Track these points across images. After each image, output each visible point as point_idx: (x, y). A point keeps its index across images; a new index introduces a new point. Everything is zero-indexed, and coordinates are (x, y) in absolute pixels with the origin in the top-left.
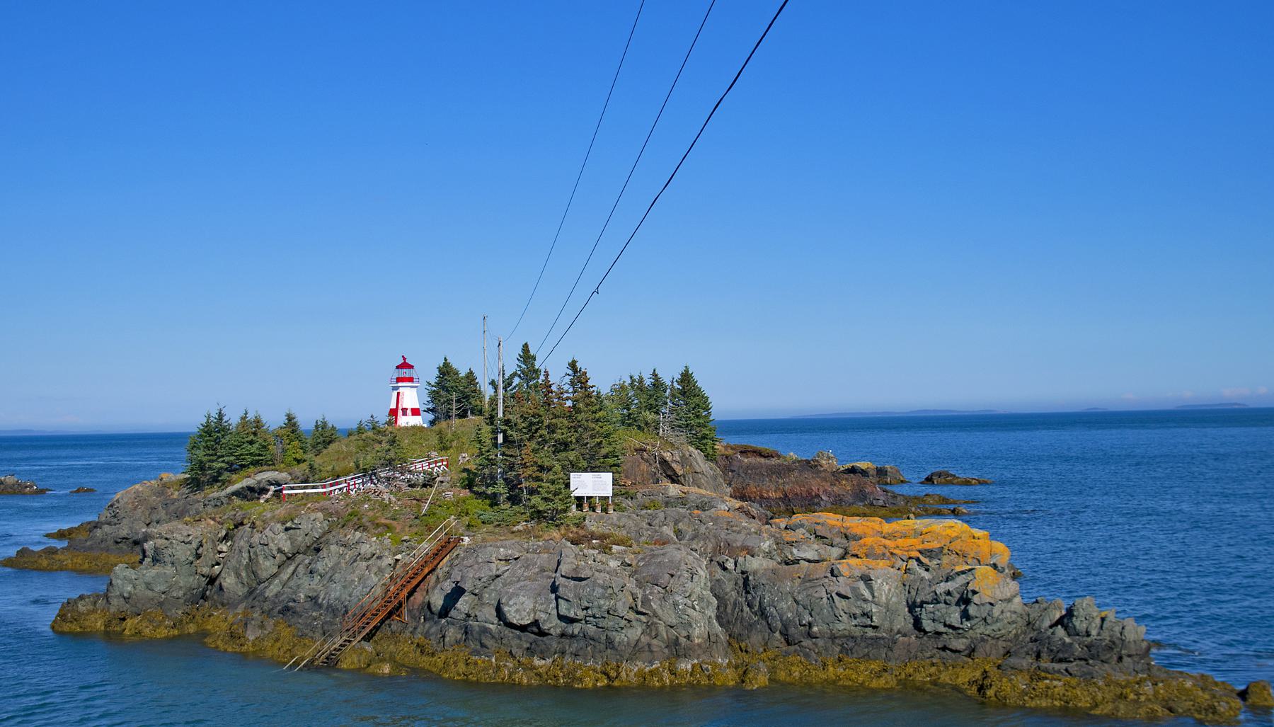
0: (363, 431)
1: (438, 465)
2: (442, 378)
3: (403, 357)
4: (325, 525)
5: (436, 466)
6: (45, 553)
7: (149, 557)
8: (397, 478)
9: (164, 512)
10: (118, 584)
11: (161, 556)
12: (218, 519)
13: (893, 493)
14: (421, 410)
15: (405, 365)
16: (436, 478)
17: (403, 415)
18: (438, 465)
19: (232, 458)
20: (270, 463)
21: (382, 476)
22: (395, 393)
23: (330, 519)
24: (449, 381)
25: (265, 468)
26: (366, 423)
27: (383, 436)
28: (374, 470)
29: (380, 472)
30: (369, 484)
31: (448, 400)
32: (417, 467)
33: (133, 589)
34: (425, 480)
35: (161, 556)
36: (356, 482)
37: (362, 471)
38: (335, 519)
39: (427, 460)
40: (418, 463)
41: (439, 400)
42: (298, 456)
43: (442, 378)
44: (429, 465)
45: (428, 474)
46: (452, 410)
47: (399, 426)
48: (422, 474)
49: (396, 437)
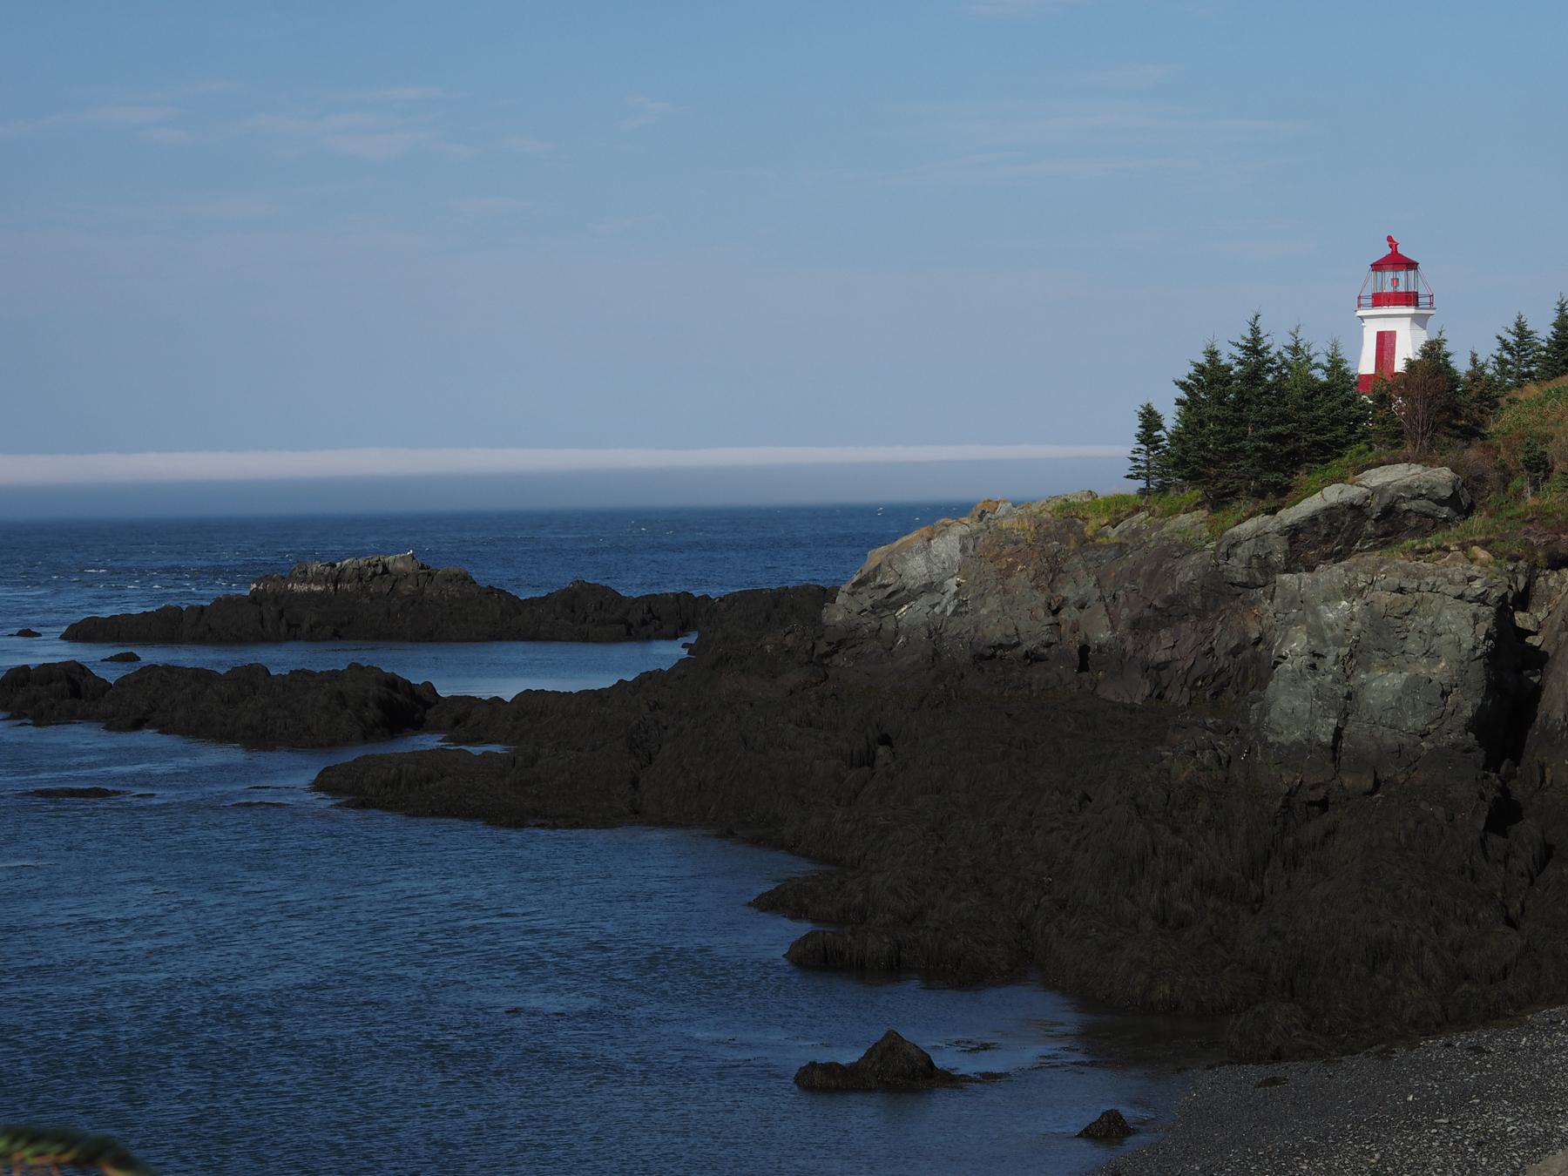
3: (1390, 239)
15: (1396, 261)
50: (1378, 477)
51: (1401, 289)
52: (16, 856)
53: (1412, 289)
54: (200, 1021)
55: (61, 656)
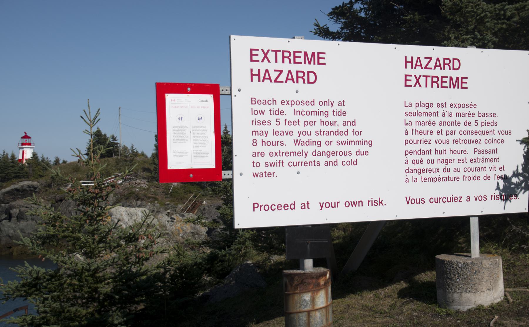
3: (25, 132)
4: (114, 199)
7: (15, 217)
10: (5, 230)
11: (25, 216)
12: (46, 199)
15: (26, 137)
19: (4, 175)
20: (26, 177)
22: (21, 151)
23: (117, 196)
25: (23, 179)
33: (13, 232)
35: (25, 216)
38: (119, 196)
42: (41, 174)
50: (21, 184)
51: (27, 142)
52: (189, 208)
53: (30, 142)
54: (460, 279)
55: (97, 123)
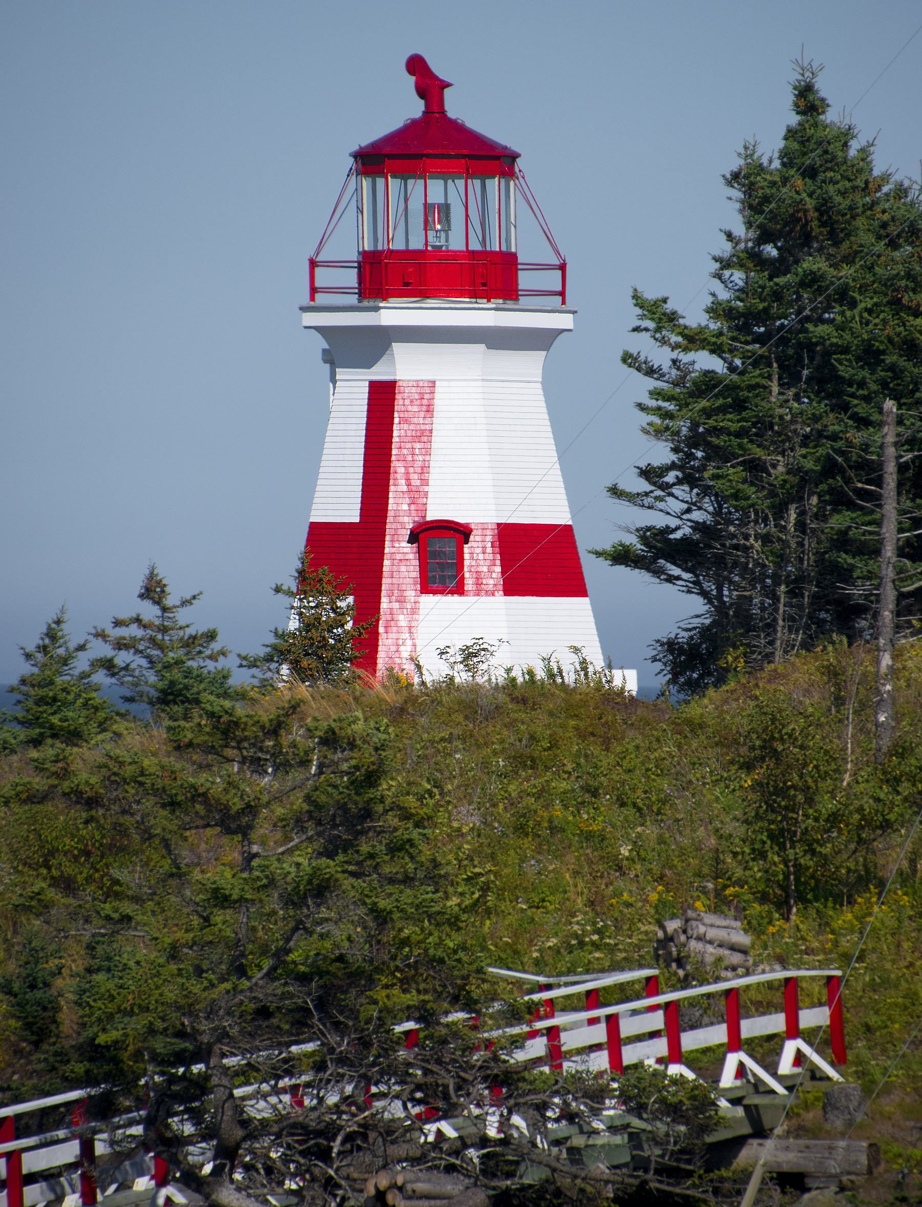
0: (74, 715)
1: (751, 1028)
2: (778, 267)
3: (416, 65)
5: (735, 1043)
6: (707, 980)
8: (390, 1131)
9: (868, 919)
13: (773, 653)
14: (584, 543)
16: (739, 1142)
17: (426, 588)
18: (751, 1028)
21: (259, 1110)
24: (843, 296)
26: (102, 650)
27: (257, 766)
28: (186, 1059)
29: (245, 1074)
30: (143, 1184)
31: (830, 468)
32: (569, 1041)
34: (640, 1164)
36: (32, 1162)
37: (80, 1068)
39: (651, 986)
40: (570, 1004)
41: (755, 467)
43: (778, 267)
44: (673, 1031)
45: (673, 1111)
46: (875, 551)
47: (393, 677)
48: (612, 1110)
49: (372, 778)
